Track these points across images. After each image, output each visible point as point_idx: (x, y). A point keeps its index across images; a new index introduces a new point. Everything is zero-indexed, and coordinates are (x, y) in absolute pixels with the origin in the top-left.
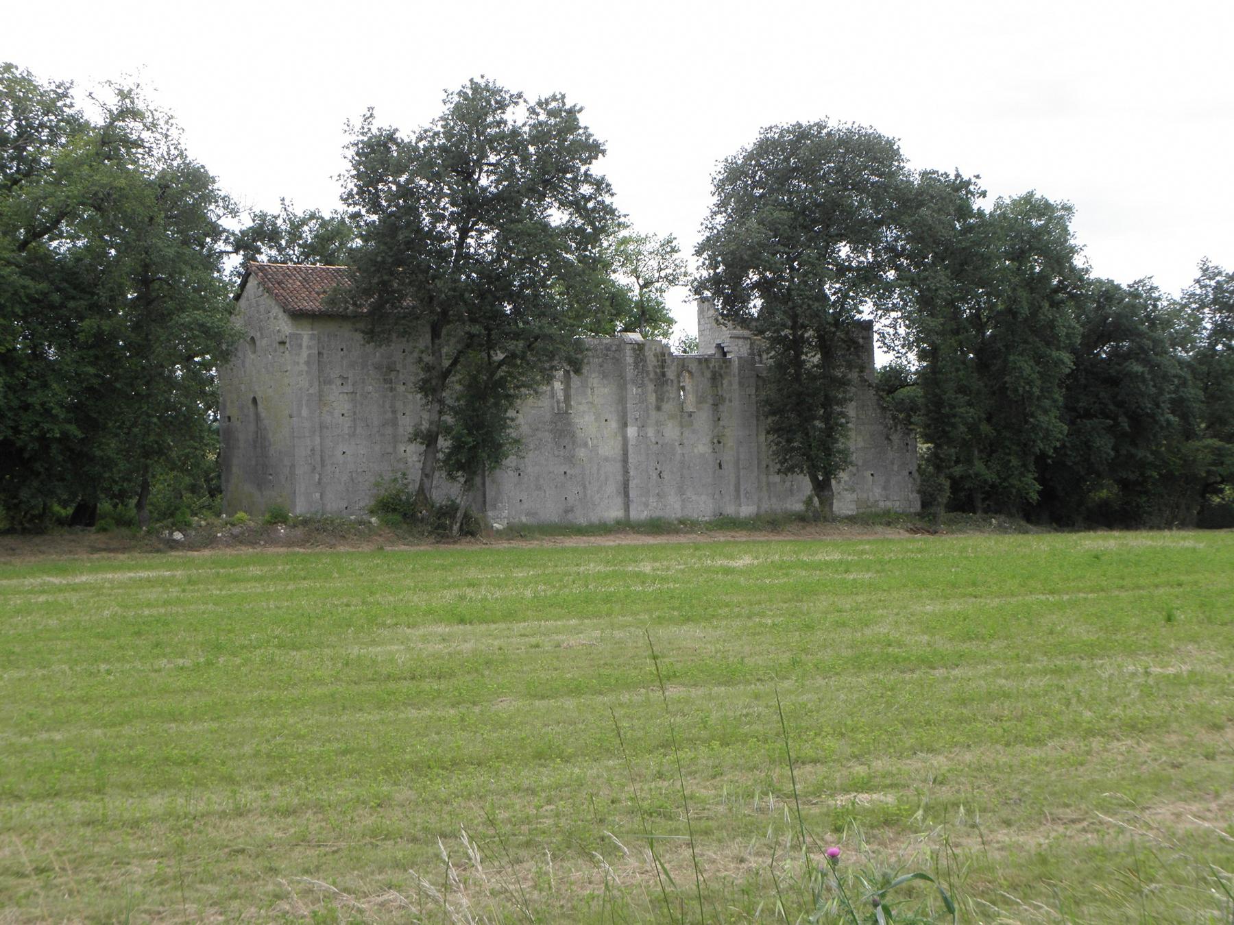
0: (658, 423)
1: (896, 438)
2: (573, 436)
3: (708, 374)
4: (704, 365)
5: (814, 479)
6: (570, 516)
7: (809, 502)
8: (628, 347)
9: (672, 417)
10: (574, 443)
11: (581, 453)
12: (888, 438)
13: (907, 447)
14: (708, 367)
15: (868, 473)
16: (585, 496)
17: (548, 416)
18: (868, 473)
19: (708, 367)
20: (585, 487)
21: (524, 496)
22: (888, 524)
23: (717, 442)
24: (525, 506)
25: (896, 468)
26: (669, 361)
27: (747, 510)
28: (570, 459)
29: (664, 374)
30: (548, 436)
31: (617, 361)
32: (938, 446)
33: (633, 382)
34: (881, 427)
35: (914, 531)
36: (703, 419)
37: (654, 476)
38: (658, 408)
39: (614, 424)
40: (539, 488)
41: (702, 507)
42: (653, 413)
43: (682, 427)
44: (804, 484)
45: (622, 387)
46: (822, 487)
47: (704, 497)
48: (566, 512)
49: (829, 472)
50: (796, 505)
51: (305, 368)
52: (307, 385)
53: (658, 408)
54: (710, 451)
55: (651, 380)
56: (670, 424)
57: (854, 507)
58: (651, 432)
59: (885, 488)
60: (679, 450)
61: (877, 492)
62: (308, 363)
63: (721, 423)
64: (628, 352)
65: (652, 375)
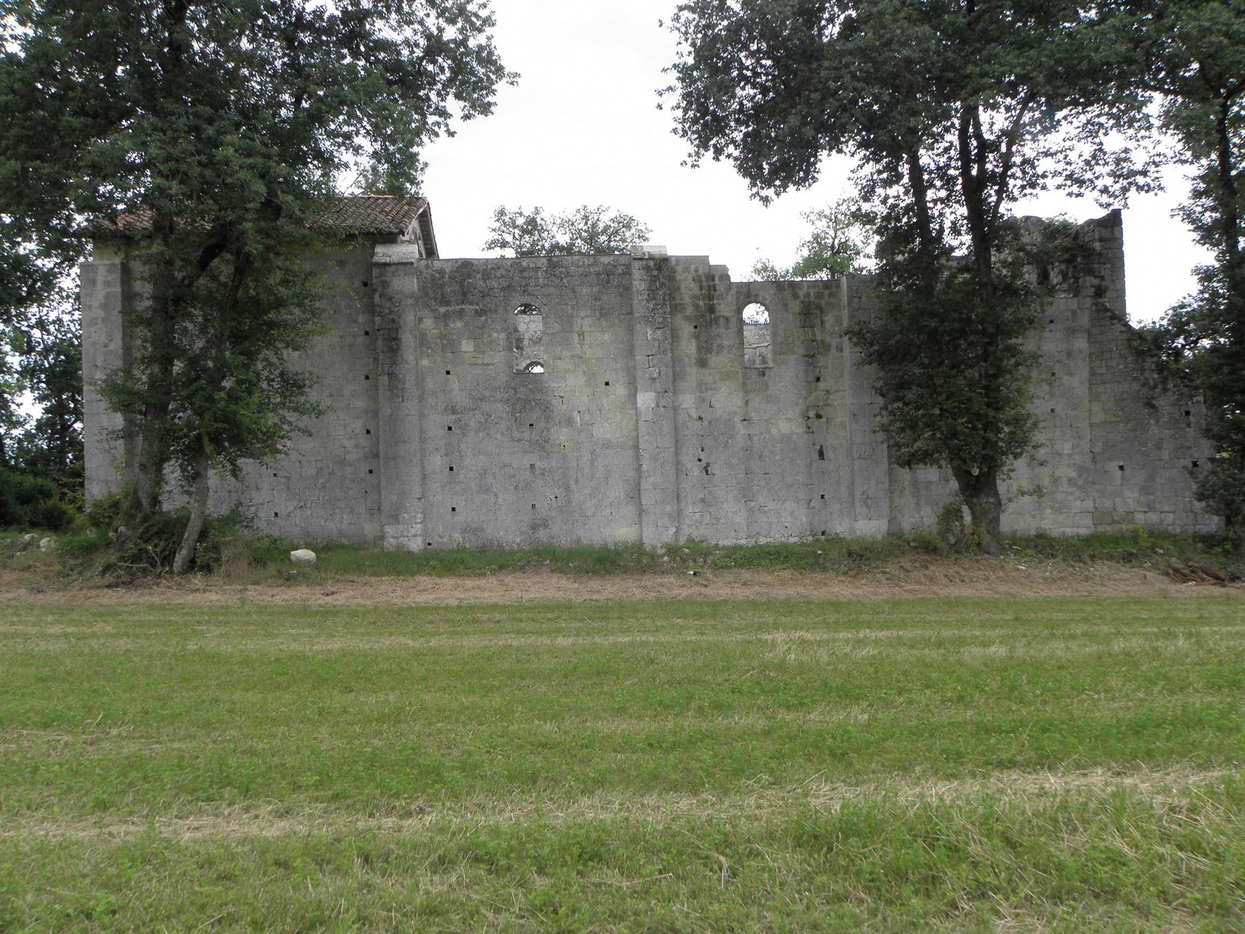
0: (701, 386)
1: (1165, 403)
2: (547, 409)
3: (795, 306)
4: (788, 293)
5: (962, 474)
6: (542, 534)
7: (950, 515)
8: (637, 264)
9: (727, 376)
10: (548, 419)
11: (562, 435)
12: (1149, 404)
13: (566, 224)
14: (796, 296)
15: (1116, 464)
16: (569, 502)
17: (502, 379)
18: (1115, 465)
19: (796, 296)
20: (568, 489)
21: (459, 502)
22: (1128, 558)
23: (815, 416)
24: (460, 517)
25: (1165, 455)
26: (721, 289)
27: (869, 527)
28: (542, 445)
29: (712, 309)
30: (500, 409)
31: (626, 290)
32: (341, 20)
33: (647, 321)
34: (1136, 386)
35: (1180, 576)
36: (787, 379)
37: (696, 470)
38: (702, 363)
39: (620, 390)
40: (485, 490)
41: (785, 522)
42: (693, 372)
43: (747, 392)
44: (939, 482)
45: (630, 330)
46: (978, 485)
47: (789, 506)
48: (534, 527)
49: (991, 466)
50: (921, 517)
51: (101, 314)
52: (103, 339)
53: (702, 363)
54: (801, 430)
55: (687, 318)
56: (724, 388)
57: (1088, 521)
58: (688, 401)
59: (1145, 490)
60: (742, 430)
61: (1131, 498)
62: (105, 307)
63: (822, 385)
64: (637, 273)
65: (689, 311)
